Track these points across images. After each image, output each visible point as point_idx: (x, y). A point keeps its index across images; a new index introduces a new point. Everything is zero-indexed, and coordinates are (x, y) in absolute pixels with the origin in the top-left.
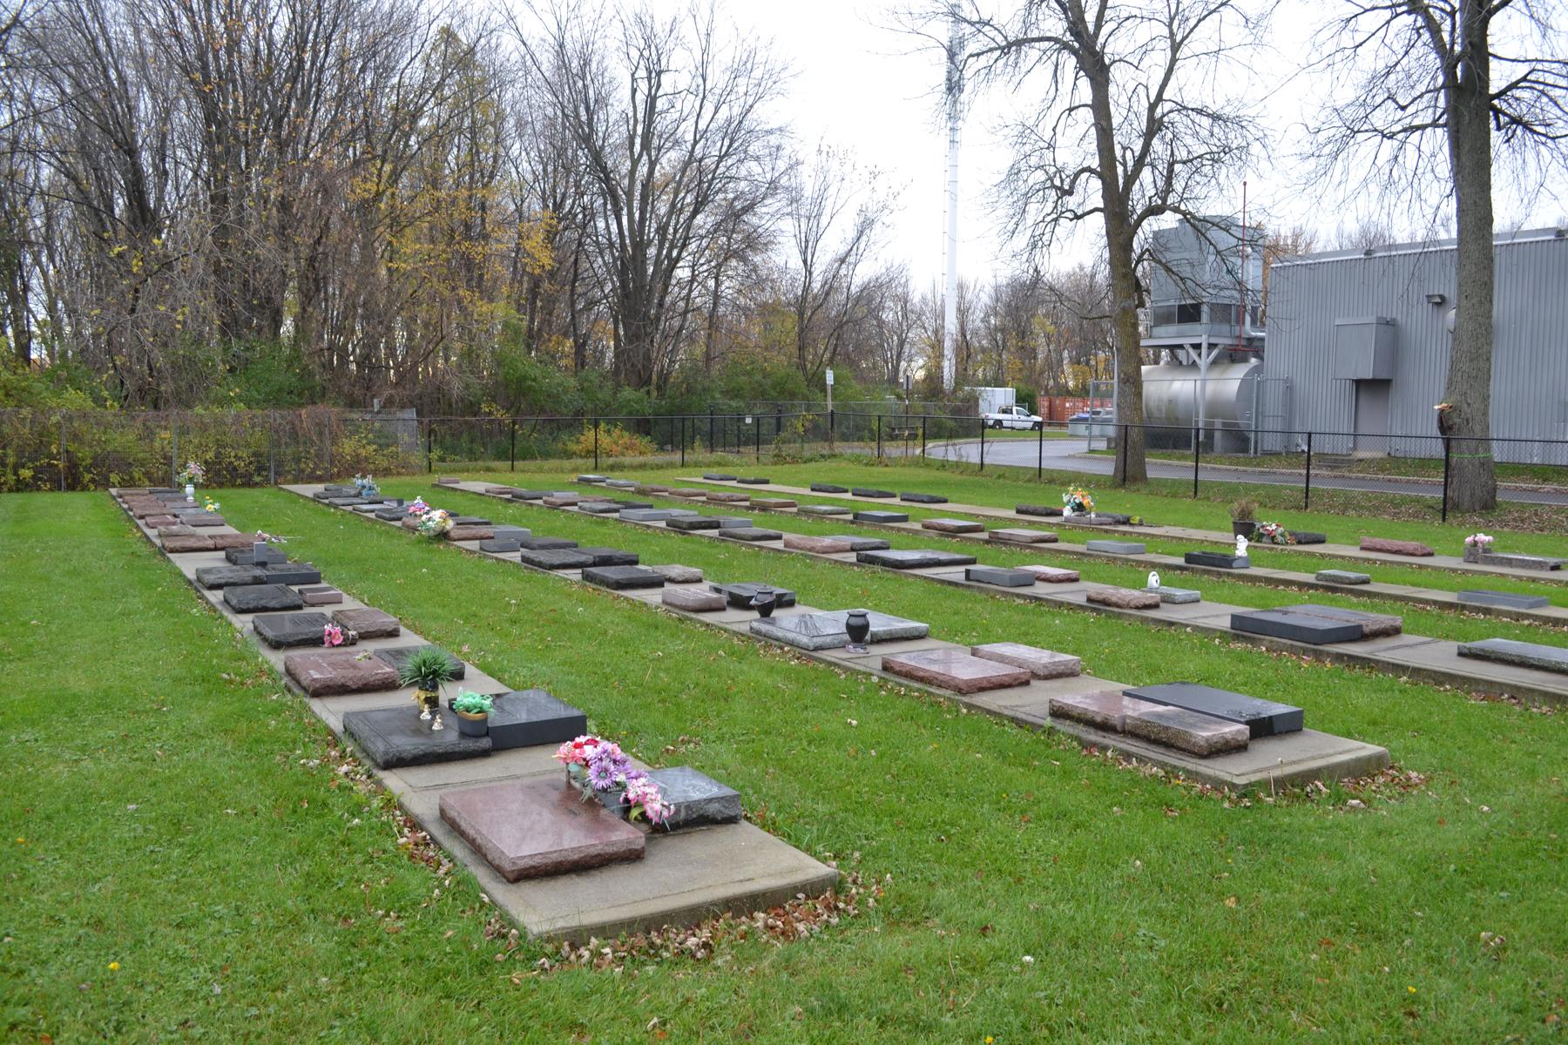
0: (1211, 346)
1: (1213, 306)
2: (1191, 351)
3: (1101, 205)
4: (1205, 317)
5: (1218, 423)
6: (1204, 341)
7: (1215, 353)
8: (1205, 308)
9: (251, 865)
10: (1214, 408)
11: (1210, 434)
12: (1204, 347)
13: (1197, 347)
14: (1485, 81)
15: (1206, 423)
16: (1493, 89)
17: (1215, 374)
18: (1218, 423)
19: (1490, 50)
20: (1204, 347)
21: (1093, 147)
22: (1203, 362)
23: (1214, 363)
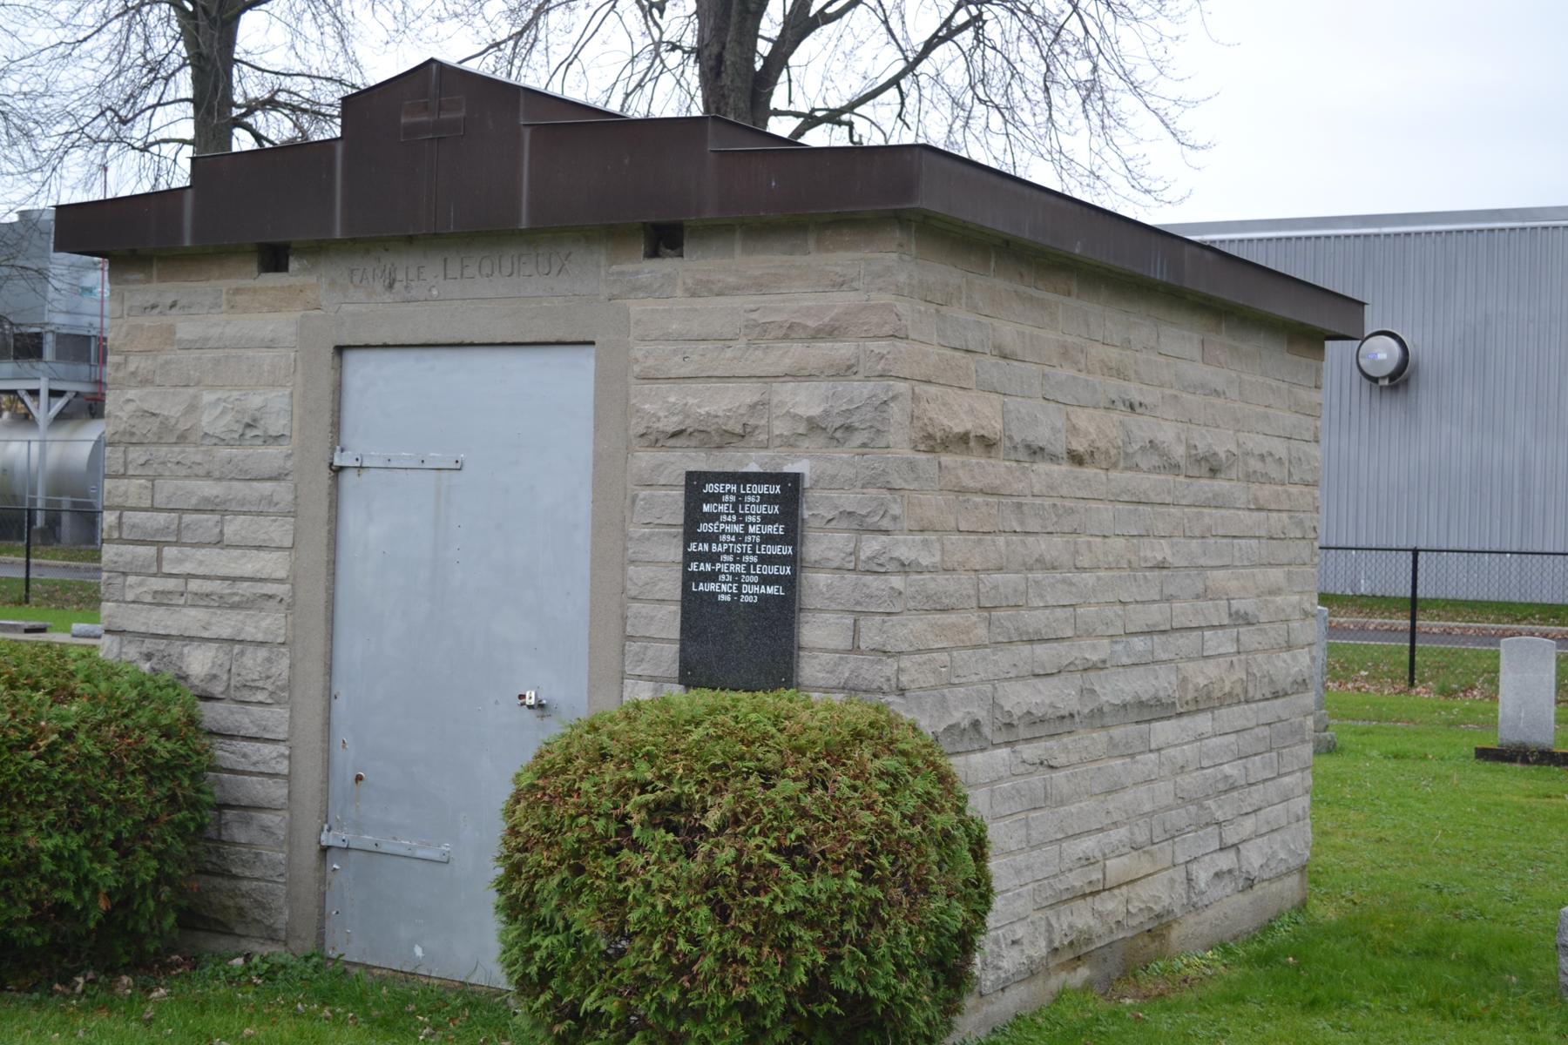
0: (55, 394)
1: (61, 338)
2: (27, 399)
3: (190, 94)
4: (49, 351)
5: (66, 502)
6: (43, 386)
7: (59, 404)
8: (49, 340)
9: (37, 122)
10: (61, 481)
11: (53, 521)
12: (44, 394)
13: (34, 393)
14: (196, 79)
15: (48, 502)
16: (189, 70)
17: (63, 432)
18: (66, 502)
19: (803, 644)
20: (44, 394)
21: (1004, 169)
22: (43, 411)
23: (61, 417)
